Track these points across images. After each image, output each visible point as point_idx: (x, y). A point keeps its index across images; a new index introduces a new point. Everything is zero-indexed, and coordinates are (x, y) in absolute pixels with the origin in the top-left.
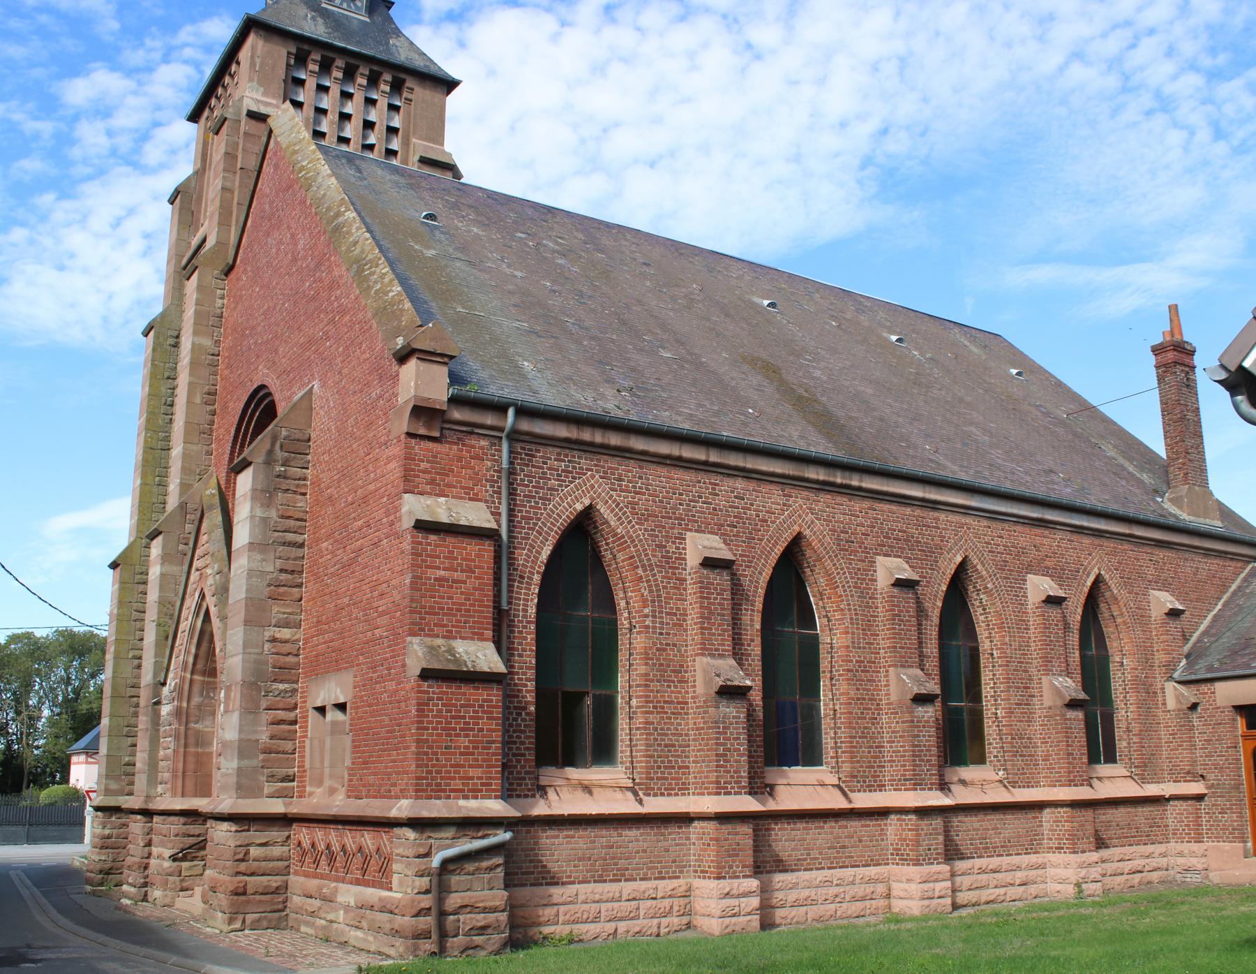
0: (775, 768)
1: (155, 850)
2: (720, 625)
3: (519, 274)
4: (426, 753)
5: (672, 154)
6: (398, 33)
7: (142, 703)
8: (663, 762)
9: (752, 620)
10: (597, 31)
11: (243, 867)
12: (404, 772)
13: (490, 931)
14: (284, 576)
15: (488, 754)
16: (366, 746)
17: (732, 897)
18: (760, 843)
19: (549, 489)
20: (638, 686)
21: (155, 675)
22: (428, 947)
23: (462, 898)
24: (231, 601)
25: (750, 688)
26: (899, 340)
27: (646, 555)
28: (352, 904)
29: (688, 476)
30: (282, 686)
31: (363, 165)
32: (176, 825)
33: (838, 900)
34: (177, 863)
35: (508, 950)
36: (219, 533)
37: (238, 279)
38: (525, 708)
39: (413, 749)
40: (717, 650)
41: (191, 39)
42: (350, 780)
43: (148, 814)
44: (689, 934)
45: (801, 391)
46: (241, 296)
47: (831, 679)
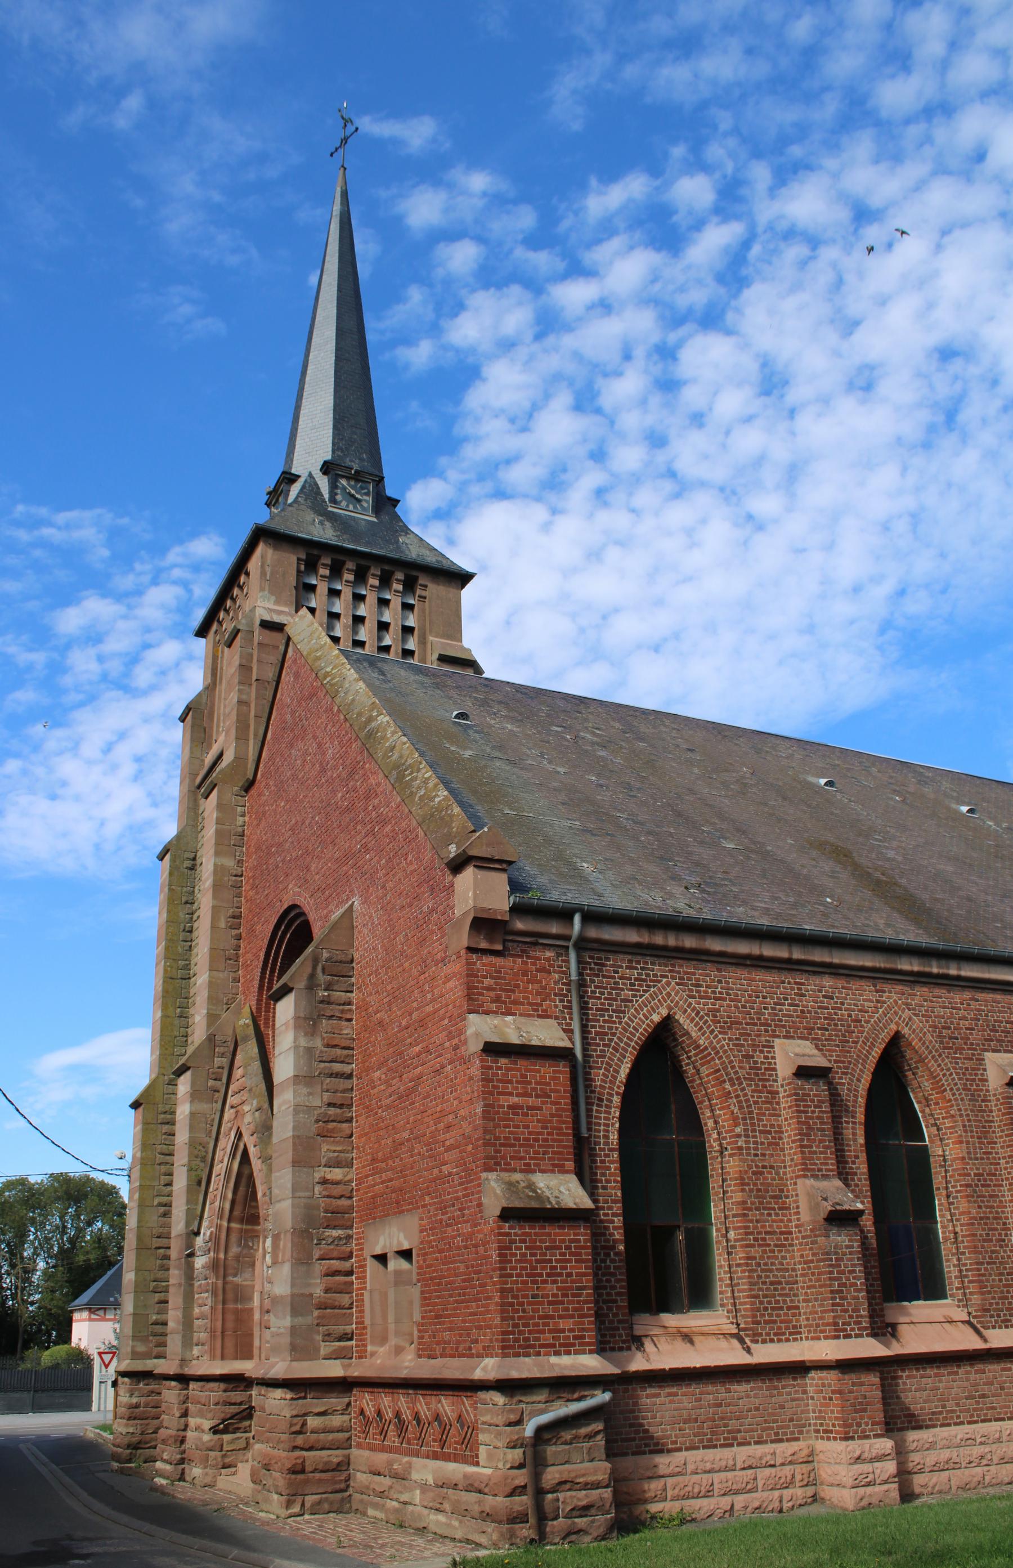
0: (894, 1304)
1: (192, 1421)
2: (820, 1141)
3: (561, 770)
4: (512, 1304)
5: (677, 636)
6: (406, 530)
7: (174, 1254)
8: (769, 1303)
9: (854, 1134)
10: (590, 516)
11: (300, 1440)
12: (490, 1327)
13: (593, 1511)
14: (332, 1111)
15: (578, 1302)
16: (438, 1297)
17: (864, 1461)
18: (888, 1396)
19: (622, 1000)
20: (734, 1216)
21: (188, 1224)
22: (525, 1532)
23: (561, 1473)
24: (275, 1140)
25: (861, 1212)
26: (970, 811)
27: (733, 1067)
28: (431, 1481)
29: (771, 977)
30: (335, 1233)
31: (386, 667)
32: (215, 1392)
33: (984, 1462)
34: (218, 1436)
35: (615, 1534)
36: (256, 1065)
37: (260, 795)
38: (613, 1248)
39: (497, 1300)
40: (820, 1170)
41: (180, 560)
42: (421, 1337)
43: (183, 1379)
44: (815, 1509)
45: (878, 874)
46: (264, 813)
47: (948, 1196)
